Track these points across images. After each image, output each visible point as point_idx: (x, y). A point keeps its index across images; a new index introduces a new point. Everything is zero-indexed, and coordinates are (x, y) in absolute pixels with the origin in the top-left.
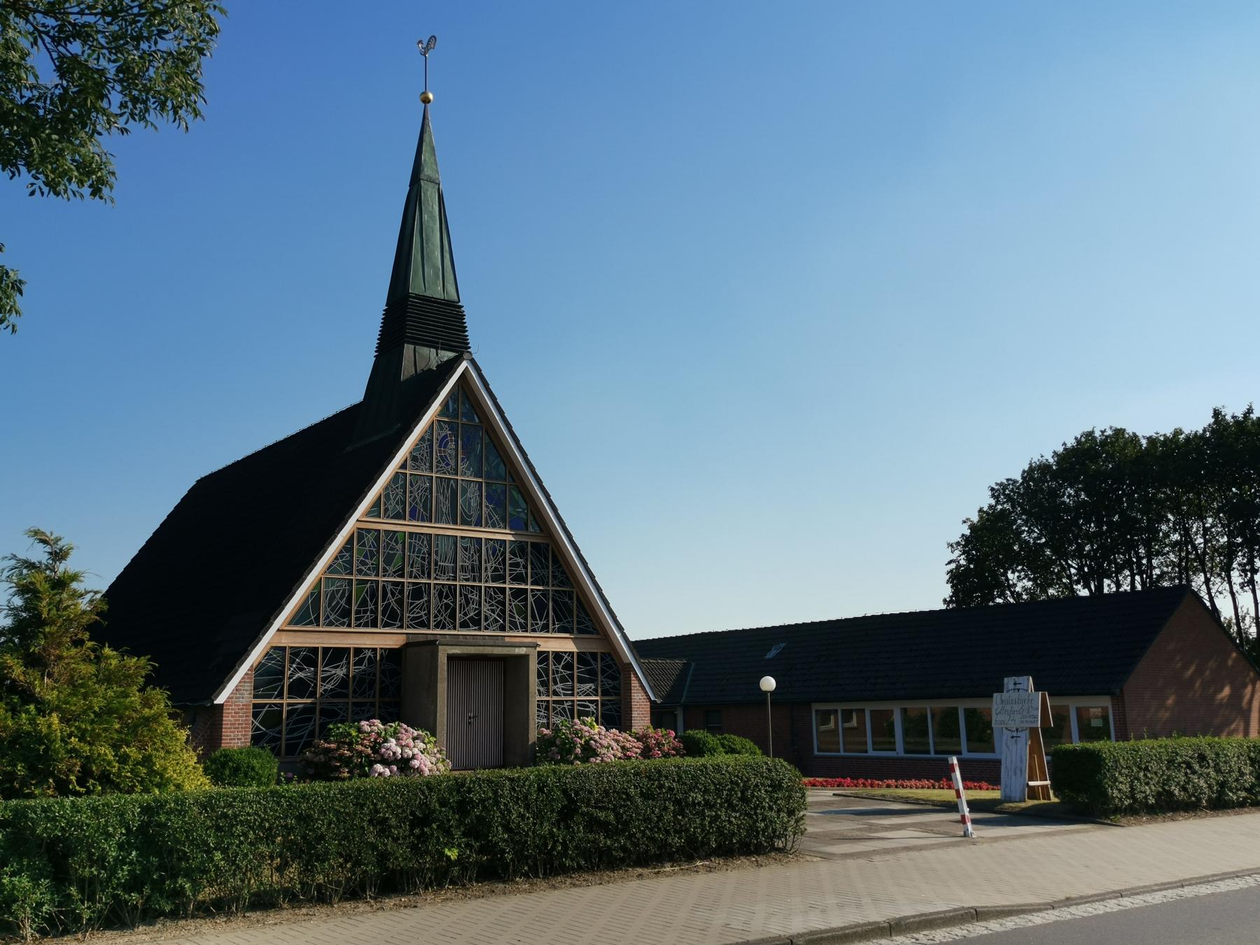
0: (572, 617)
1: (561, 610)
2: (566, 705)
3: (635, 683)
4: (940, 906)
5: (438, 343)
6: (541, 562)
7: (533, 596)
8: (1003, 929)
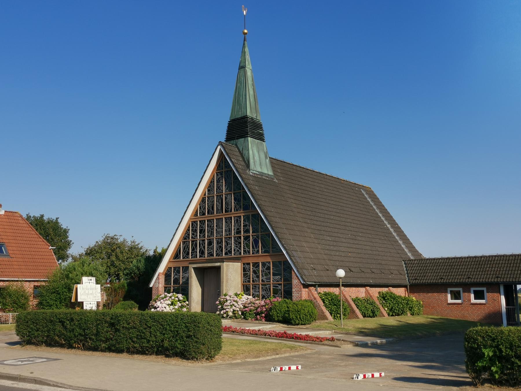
2: (267, 286)
3: (294, 276)
7: (253, 238)
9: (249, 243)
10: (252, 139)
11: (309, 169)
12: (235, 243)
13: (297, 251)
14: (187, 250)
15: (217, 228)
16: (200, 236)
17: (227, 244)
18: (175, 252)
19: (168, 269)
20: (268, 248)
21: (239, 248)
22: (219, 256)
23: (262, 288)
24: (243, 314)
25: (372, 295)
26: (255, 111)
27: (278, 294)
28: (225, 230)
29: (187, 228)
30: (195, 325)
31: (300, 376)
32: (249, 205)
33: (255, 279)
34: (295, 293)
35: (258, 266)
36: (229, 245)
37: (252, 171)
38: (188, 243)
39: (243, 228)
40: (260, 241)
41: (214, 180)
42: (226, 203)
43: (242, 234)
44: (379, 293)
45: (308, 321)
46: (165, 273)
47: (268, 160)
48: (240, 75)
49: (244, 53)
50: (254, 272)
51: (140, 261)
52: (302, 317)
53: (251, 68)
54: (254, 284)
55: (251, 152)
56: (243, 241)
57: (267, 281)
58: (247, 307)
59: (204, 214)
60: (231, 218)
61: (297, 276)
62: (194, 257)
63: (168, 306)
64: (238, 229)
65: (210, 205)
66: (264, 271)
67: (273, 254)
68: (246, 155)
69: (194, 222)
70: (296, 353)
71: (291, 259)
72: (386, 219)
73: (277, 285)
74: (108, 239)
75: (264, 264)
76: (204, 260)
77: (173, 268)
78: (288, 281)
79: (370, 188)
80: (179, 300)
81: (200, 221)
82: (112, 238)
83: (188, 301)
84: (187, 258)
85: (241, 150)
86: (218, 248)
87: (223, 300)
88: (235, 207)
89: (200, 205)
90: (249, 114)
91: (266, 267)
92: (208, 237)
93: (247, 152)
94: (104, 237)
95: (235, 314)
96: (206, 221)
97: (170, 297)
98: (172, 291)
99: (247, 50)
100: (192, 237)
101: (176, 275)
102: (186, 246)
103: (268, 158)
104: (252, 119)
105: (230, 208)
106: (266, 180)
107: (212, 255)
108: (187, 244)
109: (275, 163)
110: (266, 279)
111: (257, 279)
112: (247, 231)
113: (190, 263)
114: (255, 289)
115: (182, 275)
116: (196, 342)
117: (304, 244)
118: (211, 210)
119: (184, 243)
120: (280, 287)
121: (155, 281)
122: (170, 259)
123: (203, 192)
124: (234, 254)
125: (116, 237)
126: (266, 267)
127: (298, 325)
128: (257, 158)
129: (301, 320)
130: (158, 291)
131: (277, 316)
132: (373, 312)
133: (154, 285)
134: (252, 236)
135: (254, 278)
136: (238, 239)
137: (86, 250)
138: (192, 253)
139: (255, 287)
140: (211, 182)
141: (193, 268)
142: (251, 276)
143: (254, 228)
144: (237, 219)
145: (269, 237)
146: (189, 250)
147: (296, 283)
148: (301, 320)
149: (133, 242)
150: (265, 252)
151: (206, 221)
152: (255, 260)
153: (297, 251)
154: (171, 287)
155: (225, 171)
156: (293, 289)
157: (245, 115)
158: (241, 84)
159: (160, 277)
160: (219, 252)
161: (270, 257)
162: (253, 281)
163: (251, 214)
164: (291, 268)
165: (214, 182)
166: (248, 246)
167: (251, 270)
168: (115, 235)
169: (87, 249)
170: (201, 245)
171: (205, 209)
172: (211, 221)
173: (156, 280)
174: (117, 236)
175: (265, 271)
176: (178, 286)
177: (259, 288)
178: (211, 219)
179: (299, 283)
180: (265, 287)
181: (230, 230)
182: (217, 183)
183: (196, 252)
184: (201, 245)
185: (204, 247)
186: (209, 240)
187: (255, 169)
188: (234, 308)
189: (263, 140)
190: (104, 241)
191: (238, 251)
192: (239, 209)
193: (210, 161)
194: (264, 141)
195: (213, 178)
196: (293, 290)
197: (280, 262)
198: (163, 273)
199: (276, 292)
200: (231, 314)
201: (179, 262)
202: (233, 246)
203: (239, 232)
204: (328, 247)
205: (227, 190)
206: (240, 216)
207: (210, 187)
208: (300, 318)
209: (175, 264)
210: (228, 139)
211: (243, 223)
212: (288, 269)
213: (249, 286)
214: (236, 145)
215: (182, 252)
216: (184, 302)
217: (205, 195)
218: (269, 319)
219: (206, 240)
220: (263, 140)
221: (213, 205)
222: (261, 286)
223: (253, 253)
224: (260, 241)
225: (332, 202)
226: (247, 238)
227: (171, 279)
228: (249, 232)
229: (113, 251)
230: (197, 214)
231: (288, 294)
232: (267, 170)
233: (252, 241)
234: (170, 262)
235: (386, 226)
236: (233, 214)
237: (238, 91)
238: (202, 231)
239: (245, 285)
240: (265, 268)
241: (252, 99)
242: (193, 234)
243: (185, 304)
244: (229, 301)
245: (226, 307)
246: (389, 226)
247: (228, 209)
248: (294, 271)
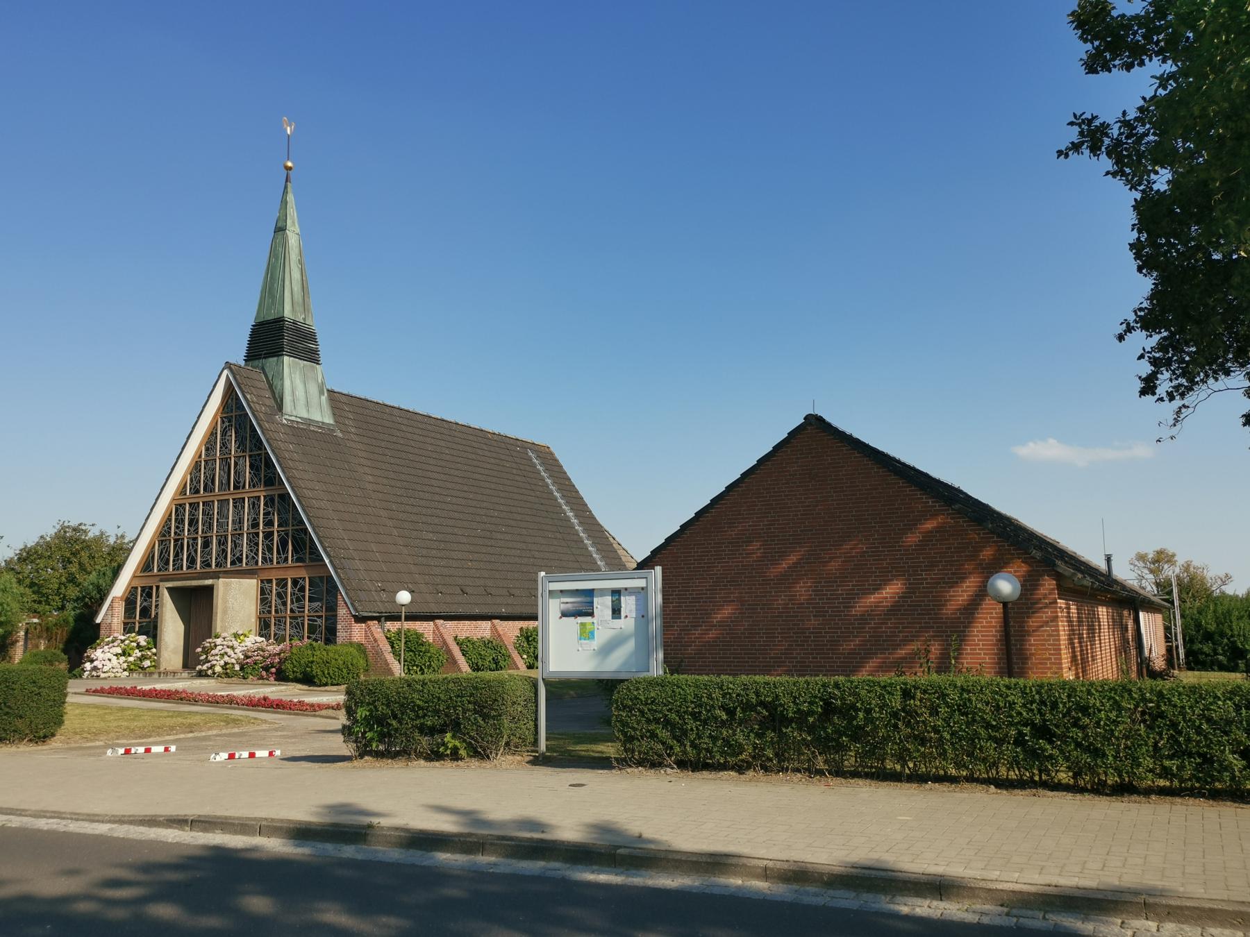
0: (306, 549)
1: (298, 543)
2: (299, 620)
3: (340, 602)
4: (85, 810)
5: (261, 355)
6: (285, 508)
7: (279, 536)
8: (1182, 926)
9: (273, 544)
10: (292, 358)
11: (421, 413)
13: (354, 559)
16: (189, 530)
17: (235, 545)
18: (144, 560)
20: (304, 554)
21: (255, 554)
23: (291, 623)
24: (242, 669)
25: (501, 633)
26: (302, 309)
28: (233, 520)
29: (167, 516)
30: (7, 687)
31: (142, 761)
32: (275, 478)
35: (286, 585)
36: (238, 548)
37: (287, 417)
42: (235, 473)
43: (261, 528)
44: (521, 629)
45: (343, 678)
47: (324, 398)
48: (276, 243)
49: (284, 203)
50: (279, 595)
51: (104, 574)
52: (331, 672)
53: (298, 230)
55: (287, 383)
57: (299, 612)
58: (250, 657)
59: (197, 491)
60: (244, 499)
61: (346, 603)
62: (178, 570)
63: (115, 657)
64: (255, 519)
67: (310, 564)
68: (279, 387)
69: (180, 505)
70: (236, 730)
71: (336, 572)
72: (556, 500)
74: (65, 532)
75: (295, 582)
76: (195, 575)
77: (139, 589)
78: (332, 609)
79: (548, 448)
80: (139, 646)
81: (190, 504)
82: (75, 530)
83: (156, 648)
84: (166, 569)
85: (270, 379)
87: (208, 645)
88: (252, 479)
89: (191, 474)
90: (288, 313)
92: (203, 533)
93: (279, 384)
94: (58, 527)
95: (226, 669)
96: (201, 504)
97: (123, 641)
98: (137, 629)
99: (291, 198)
100: (175, 533)
101: (146, 600)
103: (326, 394)
104: (295, 323)
105: (242, 482)
106: (317, 432)
107: (209, 565)
109: (337, 400)
111: (282, 608)
112: (269, 523)
113: (162, 581)
116: (7, 714)
117: (374, 547)
119: (161, 542)
122: (135, 572)
123: (196, 452)
124: (246, 564)
125: (83, 528)
127: (326, 685)
128: (300, 393)
129: (331, 678)
131: (294, 672)
132: (496, 662)
134: (278, 532)
136: (254, 537)
137: (18, 552)
138: (174, 561)
139: (279, 621)
140: (212, 434)
141: (167, 588)
142: (274, 602)
144: (254, 502)
145: (305, 535)
146: (169, 555)
148: (331, 678)
149: (123, 537)
150: (298, 560)
151: (201, 504)
152: (281, 575)
153: (354, 559)
154: (134, 623)
157: (279, 316)
158: (277, 259)
159: (116, 605)
162: (276, 611)
164: (336, 587)
165: (216, 433)
166: (270, 549)
167: (274, 592)
168: (81, 524)
169: (21, 550)
171: (200, 482)
174: (85, 525)
176: (147, 620)
177: (285, 623)
181: (241, 521)
183: (182, 560)
185: (196, 551)
186: (205, 537)
187: (295, 414)
188: (226, 658)
189: (317, 362)
190: (57, 536)
191: (253, 558)
193: (209, 397)
194: (318, 364)
195: (215, 428)
196: (339, 627)
197: (321, 578)
198: (121, 598)
199: (312, 630)
200: (218, 669)
201: (152, 578)
202: (245, 550)
203: (255, 525)
204: (424, 552)
205: (239, 450)
206: (259, 497)
207: (209, 443)
208: (329, 674)
209: (144, 582)
210: (252, 355)
211: (264, 509)
212: (332, 590)
214: (263, 369)
216: (149, 649)
217: (200, 456)
218: (281, 677)
219: (200, 539)
220: (317, 362)
221: (214, 475)
222: (288, 620)
223: (278, 563)
225: (456, 473)
226: (268, 535)
227: (135, 608)
228: (273, 526)
229: (74, 554)
230: (186, 491)
231: (330, 635)
232: (322, 415)
234: (134, 577)
235: (565, 514)
236: (247, 493)
237: (271, 275)
238: (193, 522)
241: (297, 288)
242: (177, 527)
243: (149, 653)
244: (219, 648)
245: (212, 658)
246: (571, 514)
247: (239, 483)
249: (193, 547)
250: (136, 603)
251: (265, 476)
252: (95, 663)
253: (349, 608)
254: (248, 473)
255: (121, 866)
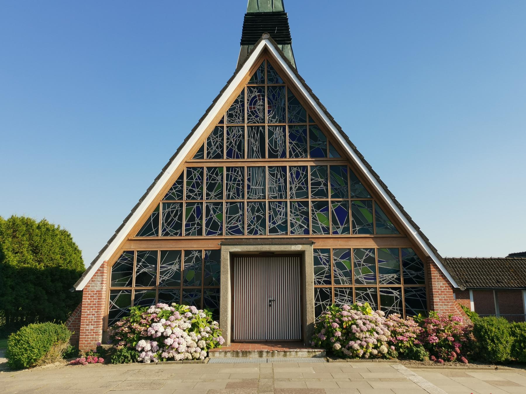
2: (369, 291)
3: (434, 273)
7: (334, 206)
12: (294, 213)
14: (176, 219)
15: (251, 184)
16: (208, 195)
19: (122, 255)
22: (256, 233)
27: (394, 306)
33: (340, 278)
34: (441, 305)
38: (177, 207)
39: (312, 188)
40: (350, 212)
41: (243, 98)
42: (271, 142)
46: (113, 263)
54: (339, 288)
56: (313, 210)
57: (367, 283)
65: (234, 142)
66: (359, 265)
73: (391, 290)
86: (254, 218)
91: (364, 258)
100: (188, 197)
102: (172, 212)
108: (175, 208)
110: (365, 278)
114: (341, 295)
115: (161, 267)
118: (237, 150)
120: (396, 293)
121: (92, 278)
126: (364, 258)
130: (99, 299)
133: (89, 286)
135: (339, 276)
136: (299, 206)
138: (187, 225)
143: (336, 189)
146: (180, 218)
147: (441, 287)
155: (268, 87)
156: (436, 297)
160: (257, 227)
161: (374, 241)
163: (328, 164)
170: (212, 212)
172: (235, 170)
173: (94, 275)
175: (363, 265)
178: (237, 167)
179: (446, 287)
180: (362, 293)
182: (250, 104)
184: (212, 212)
186: (231, 203)
192: (301, 155)
205: (274, 120)
211: (312, 180)
213: (327, 291)
215: (163, 223)
224: (350, 212)
233: (332, 211)
234: (129, 240)
239: (319, 288)
240: (363, 260)
248: (435, 266)
249: (215, 212)
250: (132, 269)
251: (311, 147)
252: (376, 343)
253: (447, 281)
254: (288, 144)
255: (469, 376)
